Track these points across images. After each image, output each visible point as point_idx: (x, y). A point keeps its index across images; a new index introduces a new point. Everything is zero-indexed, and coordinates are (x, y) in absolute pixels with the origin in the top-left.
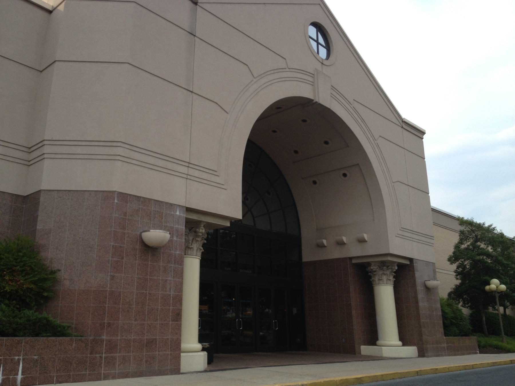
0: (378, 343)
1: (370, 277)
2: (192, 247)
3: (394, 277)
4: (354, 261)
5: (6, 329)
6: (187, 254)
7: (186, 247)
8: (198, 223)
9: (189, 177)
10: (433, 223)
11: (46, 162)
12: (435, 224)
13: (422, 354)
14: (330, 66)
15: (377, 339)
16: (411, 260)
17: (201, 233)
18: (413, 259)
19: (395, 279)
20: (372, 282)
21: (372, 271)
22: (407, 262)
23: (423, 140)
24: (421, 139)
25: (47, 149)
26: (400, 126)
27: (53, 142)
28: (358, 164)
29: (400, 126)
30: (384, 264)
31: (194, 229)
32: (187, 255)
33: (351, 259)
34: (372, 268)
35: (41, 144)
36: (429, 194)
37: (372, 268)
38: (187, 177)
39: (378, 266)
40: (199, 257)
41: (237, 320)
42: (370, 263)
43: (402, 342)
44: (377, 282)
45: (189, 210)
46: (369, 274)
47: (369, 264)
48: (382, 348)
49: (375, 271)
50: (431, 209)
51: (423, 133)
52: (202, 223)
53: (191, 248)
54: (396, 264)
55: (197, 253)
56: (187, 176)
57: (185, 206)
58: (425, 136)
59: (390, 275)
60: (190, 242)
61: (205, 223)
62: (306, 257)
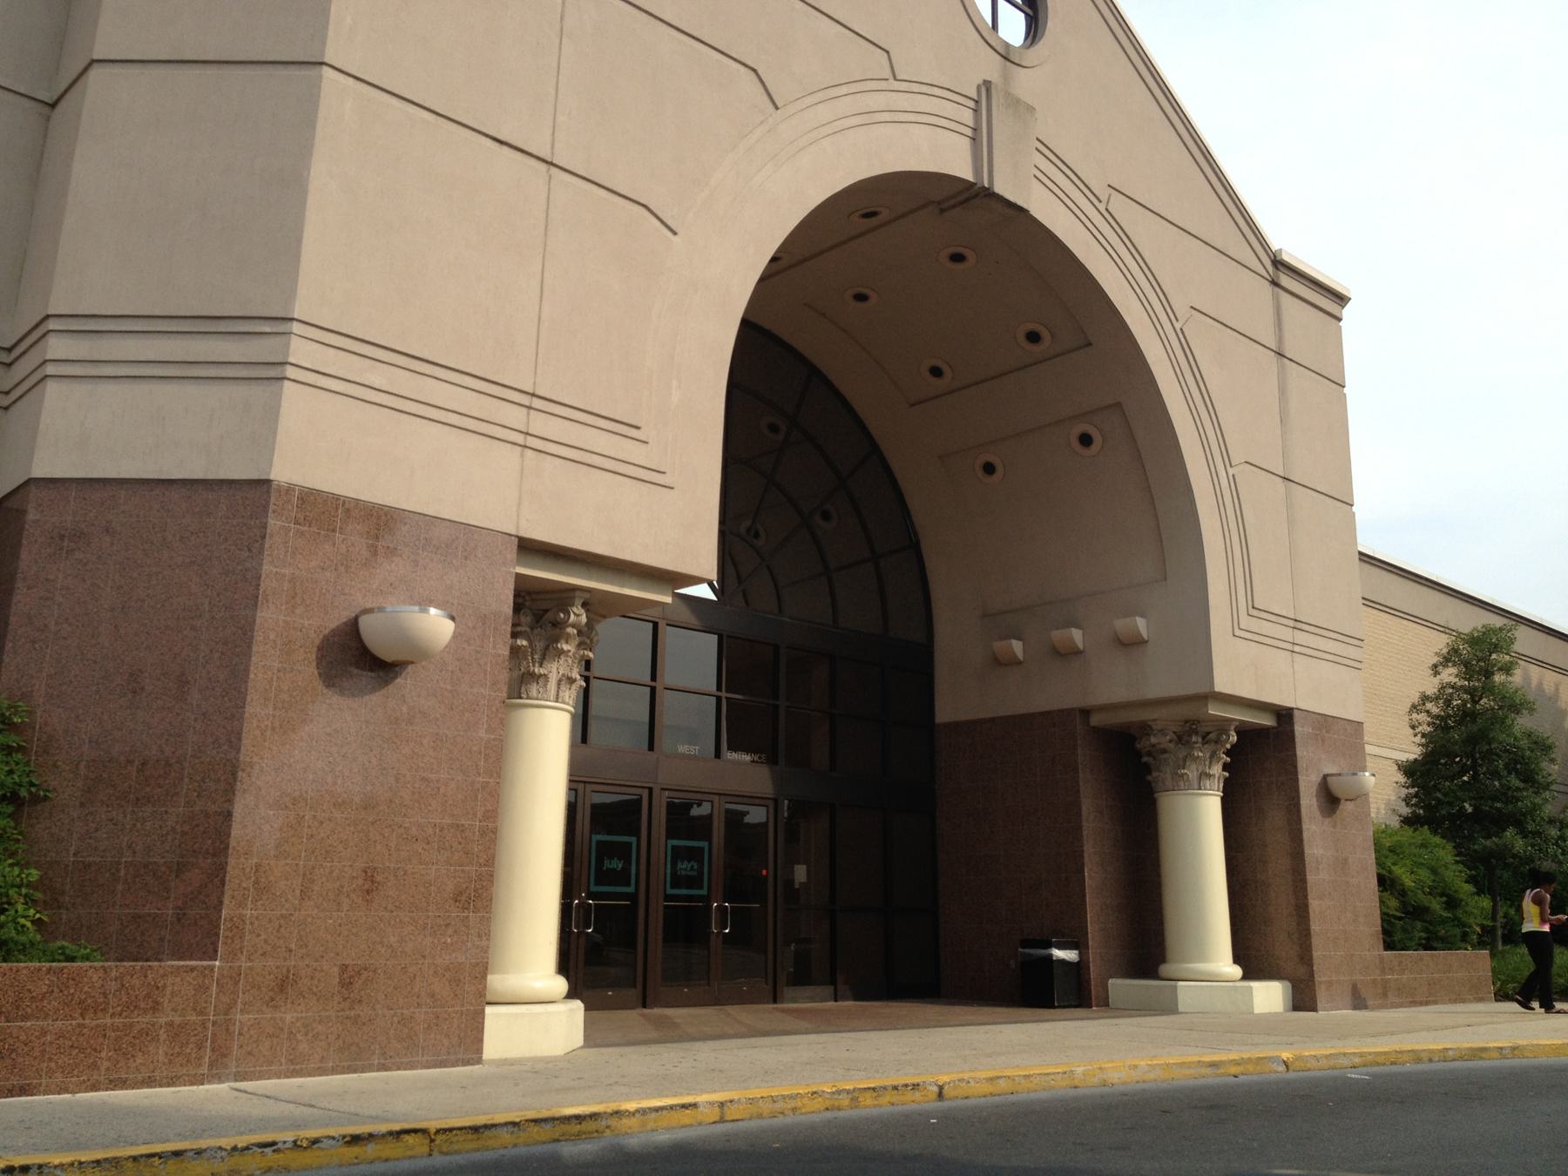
0: (1165, 969)
1: (1147, 769)
2: (542, 671)
3: (1225, 767)
4: (1095, 720)
5: (183, 941)
6: (1209, 787)
7: (1201, 774)
8: (563, 596)
9: (1297, 649)
10: (1363, 598)
11: (51, 387)
12: (1368, 602)
13: (1303, 1000)
14: (1033, 67)
15: (1162, 958)
16: (1285, 716)
17: (573, 626)
18: (1292, 709)
19: (1227, 774)
20: (1153, 785)
21: (1156, 752)
22: (1267, 721)
23: (1341, 324)
24: (1334, 321)
25: (57, 347)
26: (1267, 279)
27: (88, 324)
28: (1118, 405)
29: (1267, 279)
30: (1194, 727)
31: (549, 615)
32: (527, 699)
33: (1086, 713)
34: (1153, 740)
35: (40, 329)
36: (1352, 505)
37: (1153, 740)
38: (527, 442)
39: (1175, 732)
40: (568, 704)
41: (576, 901)
42: (1150, 723)
43: (1240, 966)
44: (1169, 783)
45: (529, 548)
46: (1145, 759)
47: (1145, 728)
48: (1176, 987)
49: (1164, 751)
50: (1357, 556)
51: (1341, 299)
52: (578, 593)
53: (541, 675)
54: (1233, 728)
55: (561, 694)
56: (525, 439)
57: (513, 532)
58: (1347, 312)
59: (1210, 763)
60: (1207, 763)
61: (1237, 724)
62: (946, 711)
